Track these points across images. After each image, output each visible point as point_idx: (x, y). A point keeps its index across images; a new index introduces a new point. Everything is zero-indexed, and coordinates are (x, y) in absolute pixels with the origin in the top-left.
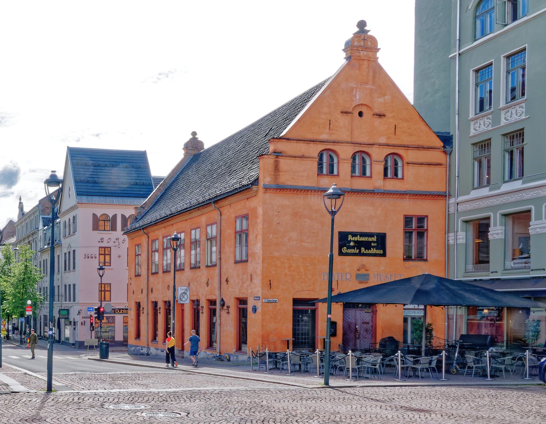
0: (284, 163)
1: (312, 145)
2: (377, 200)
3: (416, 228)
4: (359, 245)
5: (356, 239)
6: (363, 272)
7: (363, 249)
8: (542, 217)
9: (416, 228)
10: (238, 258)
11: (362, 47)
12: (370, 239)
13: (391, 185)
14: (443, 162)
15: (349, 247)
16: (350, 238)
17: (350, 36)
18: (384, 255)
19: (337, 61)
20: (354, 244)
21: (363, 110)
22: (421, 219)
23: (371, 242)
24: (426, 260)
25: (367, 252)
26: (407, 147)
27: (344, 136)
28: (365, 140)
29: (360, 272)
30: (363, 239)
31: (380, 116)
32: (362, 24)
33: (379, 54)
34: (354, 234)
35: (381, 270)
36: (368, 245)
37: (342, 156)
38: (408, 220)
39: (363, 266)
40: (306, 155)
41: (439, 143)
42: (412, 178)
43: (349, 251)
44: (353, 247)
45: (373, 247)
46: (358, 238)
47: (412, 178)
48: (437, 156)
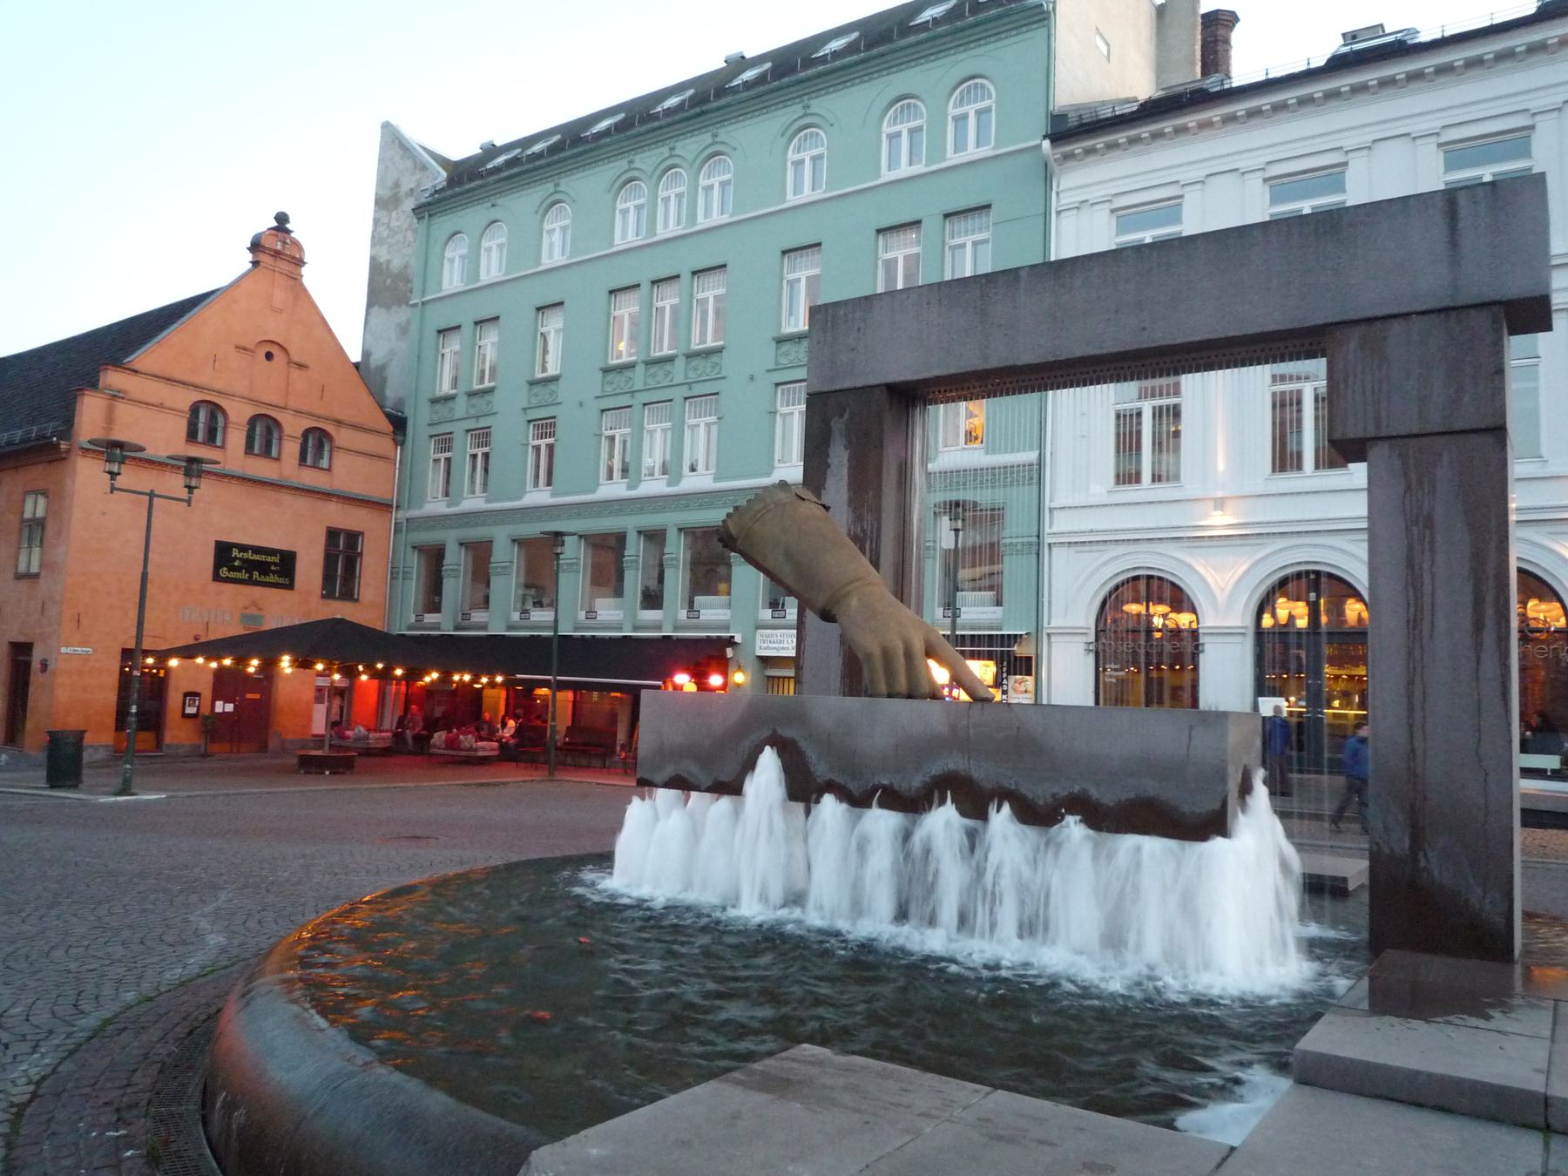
0: (122, 409)
1: (179, 390)
2: (287, 498)
3: (343, 554)
4: (250, 566)
5: (245, 555)
6: (253, 611)
7: (256, 575)
8: (1129, 231)
9: (343, 554)
10: (22, 568)
11: (276, 250)
12: (270, 559)
13: (309, 478)
14: (390, 454)
15: (232, 569)
16: (235, 552)
17: (264, 229)
18: (290, 586)
19: (228, 263)
20: (238, 563)
21: (276, 359)
22: (353, 537)
23: (270, 564)
24: (357, 600)
25: (263, 579)
26: (339, 423)
27: (240, 387)
28: (274, 399)
29: (248, 612)
30: (257, 557)
31: (301, 366)
32: (282, 219)
33: (304, 270)
34: (243, 548)
35: (281, 609)
36: (263, 568)
37: (232, 416)
38: (332, 534)
39: (255, 604)
40: (168, 404)
41: (387, 427)
42: (347, 473)
43: (233, 575)
44: (238, 569)
45: (274, 572)
46: (249, 555)
47: (347, 473)
48: (384, 445)
